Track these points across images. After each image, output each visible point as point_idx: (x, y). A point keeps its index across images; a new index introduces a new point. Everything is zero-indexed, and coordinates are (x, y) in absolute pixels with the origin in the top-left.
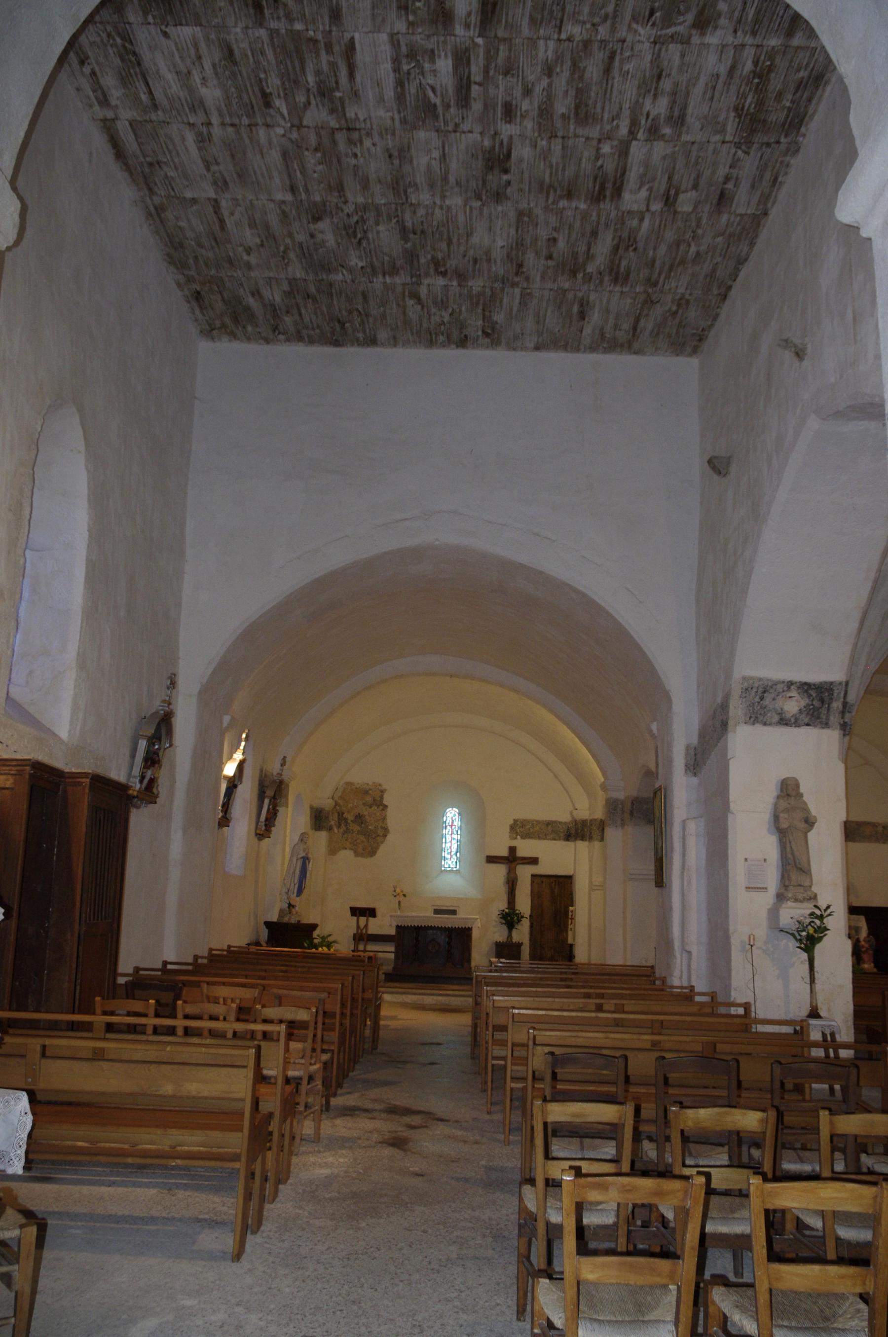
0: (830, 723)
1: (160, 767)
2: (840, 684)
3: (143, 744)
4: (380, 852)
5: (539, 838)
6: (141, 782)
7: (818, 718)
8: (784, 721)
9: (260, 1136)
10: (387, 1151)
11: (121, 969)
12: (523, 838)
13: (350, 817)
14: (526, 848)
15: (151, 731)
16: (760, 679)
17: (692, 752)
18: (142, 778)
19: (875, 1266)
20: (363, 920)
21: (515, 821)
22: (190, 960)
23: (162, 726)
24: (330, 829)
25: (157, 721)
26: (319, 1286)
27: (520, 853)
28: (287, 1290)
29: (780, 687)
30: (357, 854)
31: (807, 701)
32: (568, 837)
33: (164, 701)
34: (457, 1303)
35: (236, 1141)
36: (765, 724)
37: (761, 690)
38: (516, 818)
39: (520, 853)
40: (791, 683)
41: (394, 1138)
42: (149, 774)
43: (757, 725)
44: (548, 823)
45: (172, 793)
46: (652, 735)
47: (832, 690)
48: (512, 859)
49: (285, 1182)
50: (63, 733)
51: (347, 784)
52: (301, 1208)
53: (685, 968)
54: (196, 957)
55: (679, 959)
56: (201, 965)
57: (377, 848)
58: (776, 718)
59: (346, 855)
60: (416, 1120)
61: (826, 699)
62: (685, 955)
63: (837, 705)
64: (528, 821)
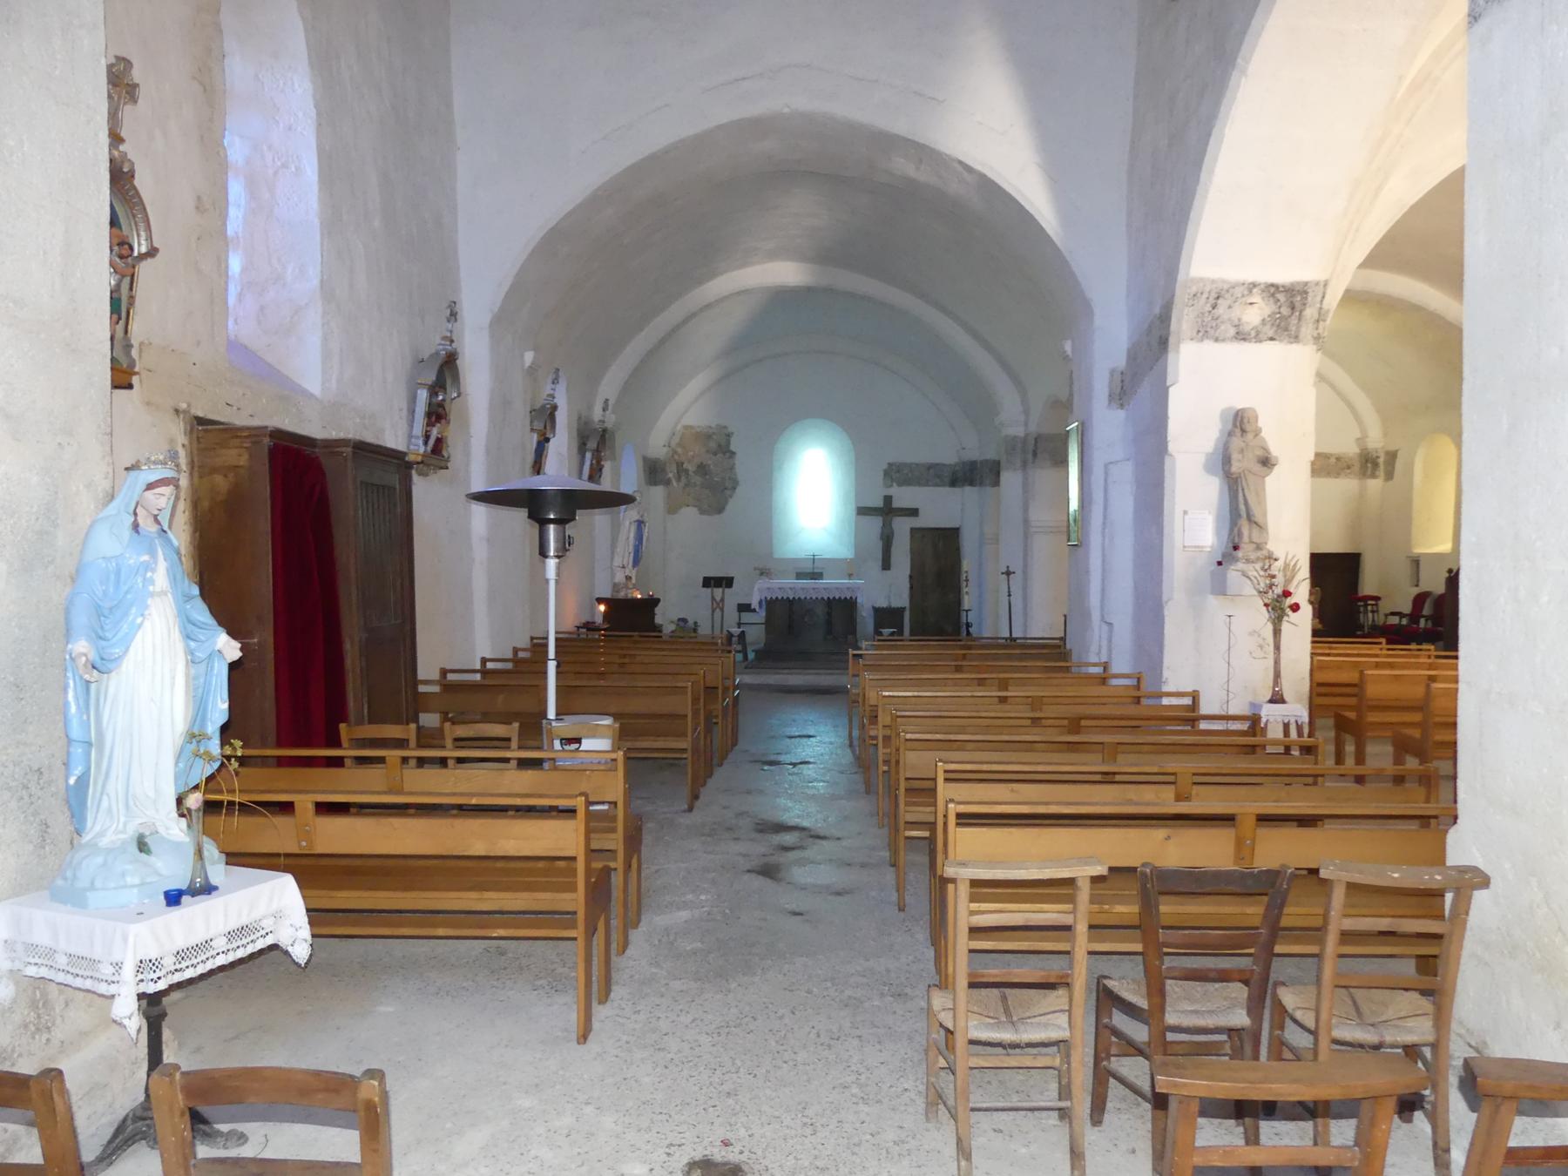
0: (1302, 335)
1: (448, 422)
2: (1317, 284)
3: (423, 395)
4: (729, 507)
5: (920, 485)
6: (426, 443)
7: (1286, 329)
8: (1241, 336)
9: (599, 891)
10: (759, 882)
11: (422, 674)
12: (900, 485)
13: (691, 468)
14: (905, 497)
15: (431, 378)
16: (1213, 281)
17: (1118, 378)
18: (427, 437)
19: (1433, 1118)
20: (718, 592)
21: (890, 465)
22: (510, 655)
23: (447, 368)
24: (667, 483)
25: (439, 362)
26: (685, 1072)
27: (896, 504)
28: (647, 1079)
29: (1238, 292)
30: (702, 512)
31: (1274, 308)
32: (954, 483)
33: (444, 338)
34: (855, 1090)
35: (575, 900)
36: (1217, 340)
37: (1214, 295)
38: (891, 461)
39: (896, 504)
40: (1254, 285)
41: (766, 865)
42: (435, 432)
43: (1206, 342)
44: (930, 467)
45: (467, 454)
46: (1066, 358)
47: (1306, 293)
48: (888, 510)
49: (636, 925)
50: (313, 382)
51: (686, 427)
52: (657, 965)
53: (1104, 643)
54: (516, 651)
55: (1097, 631)
56: (524, 661)
57: (726, 502)
58: (1232, 331)
59: (689, 514)
60: (789, 838)
61: (1298, 305)
62: (1105, 628)
63: (1310, 313)
64: (905, 465)
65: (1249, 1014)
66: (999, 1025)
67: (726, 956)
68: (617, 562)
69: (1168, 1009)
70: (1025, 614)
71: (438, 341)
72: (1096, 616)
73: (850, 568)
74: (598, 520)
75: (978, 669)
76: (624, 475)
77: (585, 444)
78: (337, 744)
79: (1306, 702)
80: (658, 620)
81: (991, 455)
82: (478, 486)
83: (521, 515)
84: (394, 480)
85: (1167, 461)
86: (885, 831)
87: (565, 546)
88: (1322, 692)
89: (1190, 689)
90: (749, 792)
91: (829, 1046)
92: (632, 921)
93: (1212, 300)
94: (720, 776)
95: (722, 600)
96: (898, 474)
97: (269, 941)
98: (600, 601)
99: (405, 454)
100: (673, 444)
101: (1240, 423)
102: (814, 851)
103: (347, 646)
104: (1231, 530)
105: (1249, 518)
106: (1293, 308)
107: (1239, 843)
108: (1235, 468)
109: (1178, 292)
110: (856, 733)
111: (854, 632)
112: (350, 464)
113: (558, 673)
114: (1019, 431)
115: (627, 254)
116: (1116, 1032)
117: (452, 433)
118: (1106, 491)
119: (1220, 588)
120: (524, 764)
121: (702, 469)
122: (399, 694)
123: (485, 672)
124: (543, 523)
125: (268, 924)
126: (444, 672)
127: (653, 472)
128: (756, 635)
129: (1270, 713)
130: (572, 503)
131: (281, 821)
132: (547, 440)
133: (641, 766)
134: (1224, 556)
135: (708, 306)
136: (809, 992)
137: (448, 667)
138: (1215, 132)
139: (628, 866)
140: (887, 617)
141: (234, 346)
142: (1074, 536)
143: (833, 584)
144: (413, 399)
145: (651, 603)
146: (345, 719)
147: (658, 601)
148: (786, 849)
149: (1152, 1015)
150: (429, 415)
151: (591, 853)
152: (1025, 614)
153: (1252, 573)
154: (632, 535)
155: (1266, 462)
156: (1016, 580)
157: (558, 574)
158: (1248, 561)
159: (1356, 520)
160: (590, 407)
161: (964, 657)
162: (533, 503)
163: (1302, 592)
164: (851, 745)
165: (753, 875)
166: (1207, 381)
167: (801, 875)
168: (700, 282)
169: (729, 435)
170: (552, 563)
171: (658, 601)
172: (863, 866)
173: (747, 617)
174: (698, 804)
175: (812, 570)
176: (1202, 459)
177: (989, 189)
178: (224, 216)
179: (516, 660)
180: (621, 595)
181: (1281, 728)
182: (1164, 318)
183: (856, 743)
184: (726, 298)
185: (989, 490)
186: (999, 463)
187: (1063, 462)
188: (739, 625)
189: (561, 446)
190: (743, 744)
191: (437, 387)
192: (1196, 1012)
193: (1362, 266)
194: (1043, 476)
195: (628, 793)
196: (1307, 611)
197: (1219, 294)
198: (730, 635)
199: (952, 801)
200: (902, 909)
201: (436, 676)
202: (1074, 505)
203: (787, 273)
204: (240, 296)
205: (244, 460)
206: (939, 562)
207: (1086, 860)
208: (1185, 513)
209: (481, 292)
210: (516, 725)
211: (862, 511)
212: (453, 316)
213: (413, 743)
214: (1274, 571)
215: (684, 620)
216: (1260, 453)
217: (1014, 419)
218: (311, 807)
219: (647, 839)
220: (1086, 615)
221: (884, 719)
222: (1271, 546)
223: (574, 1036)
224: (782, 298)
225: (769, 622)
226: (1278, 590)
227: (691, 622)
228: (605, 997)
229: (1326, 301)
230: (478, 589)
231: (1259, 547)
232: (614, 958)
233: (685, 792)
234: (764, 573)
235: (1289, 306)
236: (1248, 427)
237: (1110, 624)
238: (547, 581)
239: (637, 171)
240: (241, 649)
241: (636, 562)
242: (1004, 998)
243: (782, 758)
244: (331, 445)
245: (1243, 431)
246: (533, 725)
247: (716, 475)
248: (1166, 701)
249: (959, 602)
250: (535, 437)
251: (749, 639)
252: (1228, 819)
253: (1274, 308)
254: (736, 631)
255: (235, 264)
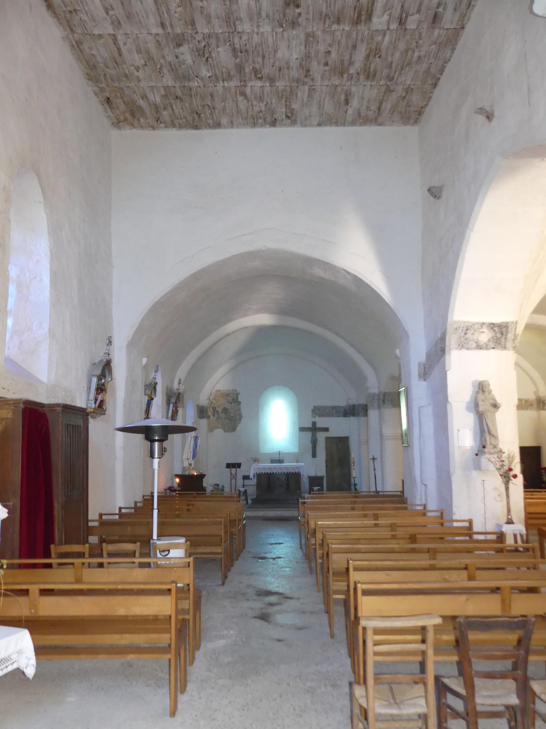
0: (507, 347)
1: (106, 393)
2: (512, 323)
3: (95, 380)
4: (238, 429)
5: (329, 416)
6: (95, 403)
8: (479, 347)
10: (259, 623)
12: (319, 416)
13: (220, 410)
14: (322, 422)
15: (99, 372)
16: (464, 322)
18: (96, 400)
20: (233, 470)
22: (133, 506)
23: (107, 367)
24: (208, 417)
27: (318, 426)
29: (476, 327)
30: (225, 431)
31: (493, 334)
33: (105, 353)
36: (468, 349)
37: (465, 329)
40: (484, 324)
42: (100, 398)
43: (463, 350)
44: (333, 408)
46: (397, 357)
52: (210, 671)
53: (423, 494)
54: (136, 503)
58: (475, 345)
59: (219, 432)
60: (273, 599)
61: (504, 332)
62: (423, 486)
63: (510, 336)
64: (321, 407)
65: (518, 697)
66: (389, 705)
67: (245, 665)
68: (185, 457)
69: (476, 695)
70: (383, 480)
71: (103, 354)
72: (418, 480)
73: (297, 457)
74: (175, 438)
75: (363, 509)
76: (187, 416)
77: (170, 400)
78: (49, 556)
79: (523, 522)
80: (204, 484)
81: (363, 401)
82: (120, 424)
83: (139, 438)
84: (80, 422)
85: (448, 405)
86: (321, 594)
87: (163, 451)
88: (531, 518)
89: (466, 518)
90: (252, 574)
91: (301, 716)
92: (197, 647)
93: (464, 331)
94: (237, 564)
95: (236, 474)
96: (318, 411)
97: (15, 666)
98: (177, 476)
99: (86, 409)
100: (211, 399)
101: (482, 387)
102: (288, 605)
103: (56, 505)
104: (481, 438)
105: (490, 433)
106: (502, 334)
107: (503, 602)
108: (481, 409)
109: (448, 328)
110: (303, 541)
111: (299, 488)
112: (60, 415)
113: (158, 514)
114: (376, 391)
115: (192, 312)
116: (449, 707)
117: (107, 397)
118: (420, 420)
119: (478, 467)
120: (142, 565)
121: (225, 410)
122: (79, 530)
123: (121, 515)
124: (152, 441)
125: (14, 657)
126: (101, 515)
127: (202, 412)
128: (252, 491)
129: (507, 529)
130: (166, 432)
131: (22, 600)
132: (152, 399)
133: (200, 563)
134: (479, 451)
135: (229, 335)
136: (289, 684)
137: (103, 513)
138: (461, 255)
139: (195, 616)
140: (315, 481)
141: (9, 361)
142: (405, 440)
143: (289, 465)
144: (90, 382)
145: (201, 477)
146: (53, 542)
147: (204, 475)
148: (272, 605)
149: (469, 699)
150: (97, 389)
151: (177, 612)
152: (430, 534)
153: (493, 460)
154: (192, 443)
155: (495, 406)
156: (378, 463)
157: (159, 467)
158: (490, 453)
159: (537, 431)
160: (172, 383)
161: (355, 502)
162: (148, 432)
163: (517, 469)
164: (301, 548)
165: (257, 619)
166: (463, 369)
167: (280, 619)
168: (225, 323)
169: (238, 394)
170: (156, 461)
171: (204, 475)
172: (311, 613)
173: (247, 482)
174: (226, 581)
175: (278, 459)
176: (465, 405)
177: (358, 281)
178: (6, 300)
179: (136, 508)
180: (187, 473)
181: (512, 536)
182: (443, 339)
183: (304, 547)
184: (237, 330)
185: (363, 419)
186: (367, 405)
187: (399, 406)
188: (244, 486)
189: (159, 400)
190: (247, 548)
191: (102, 376)
192: (490, 696)
193: (532, 313)
194: (388, 412)
195: (194, 579)
196: (520, 477)
197: (468, 328)
198: (240, 491)
199: (359, 582)
200: (332, 636)
201: (97, 518)
202: (405, 426)
203: (264, 319)
204: (11, 337)
205: (10, 416)
206: (339, 454)
207: (428, 614)
208: (459, 430)
209: (123, 331)
210: (138, 544)
211: (302, 429)
212: (110, 343)
213: (87, 555)
214: (503, 459)
215: (218, 485)
216: (492, 401)
217: (374, 385)
218: (37, 592)
219: (203, 601)
220: (414, 480)
221: (319, 536)
222: (501, 446)
223: (168, 712)
224: (261, 331)
225: (258, 485)
226: (506, 468)
227: (220, 487)
228: (183, 691)
229: (517, 330)
230: (118, 474)
231: (495, 447)
232: (188, 667)
233: (220, 575)
234: (256, 460)
235: (500, 333)
236: (485, 390)
237: (425, 485)
238: (154, 470)
239: (196, 276)
240: (8, 513)
241: (194, 456)
242: (391, 690)
243: (267, 555)
244: (52, 407)
245: (483, 391)
246: (146, 541)
247: (232, 413)
248: (455, 524)
249: (349, 473)
250: (147, 398)
251: (248, 492)
252: (496, 590)
253: (493, 334)
254: (242, 489)
255: (10, 322)
